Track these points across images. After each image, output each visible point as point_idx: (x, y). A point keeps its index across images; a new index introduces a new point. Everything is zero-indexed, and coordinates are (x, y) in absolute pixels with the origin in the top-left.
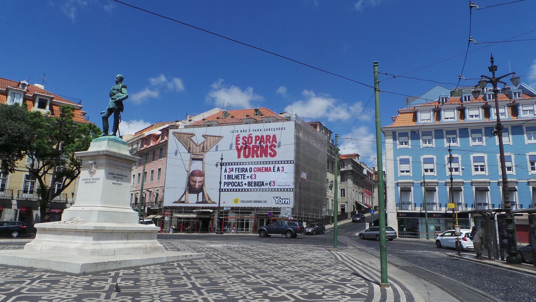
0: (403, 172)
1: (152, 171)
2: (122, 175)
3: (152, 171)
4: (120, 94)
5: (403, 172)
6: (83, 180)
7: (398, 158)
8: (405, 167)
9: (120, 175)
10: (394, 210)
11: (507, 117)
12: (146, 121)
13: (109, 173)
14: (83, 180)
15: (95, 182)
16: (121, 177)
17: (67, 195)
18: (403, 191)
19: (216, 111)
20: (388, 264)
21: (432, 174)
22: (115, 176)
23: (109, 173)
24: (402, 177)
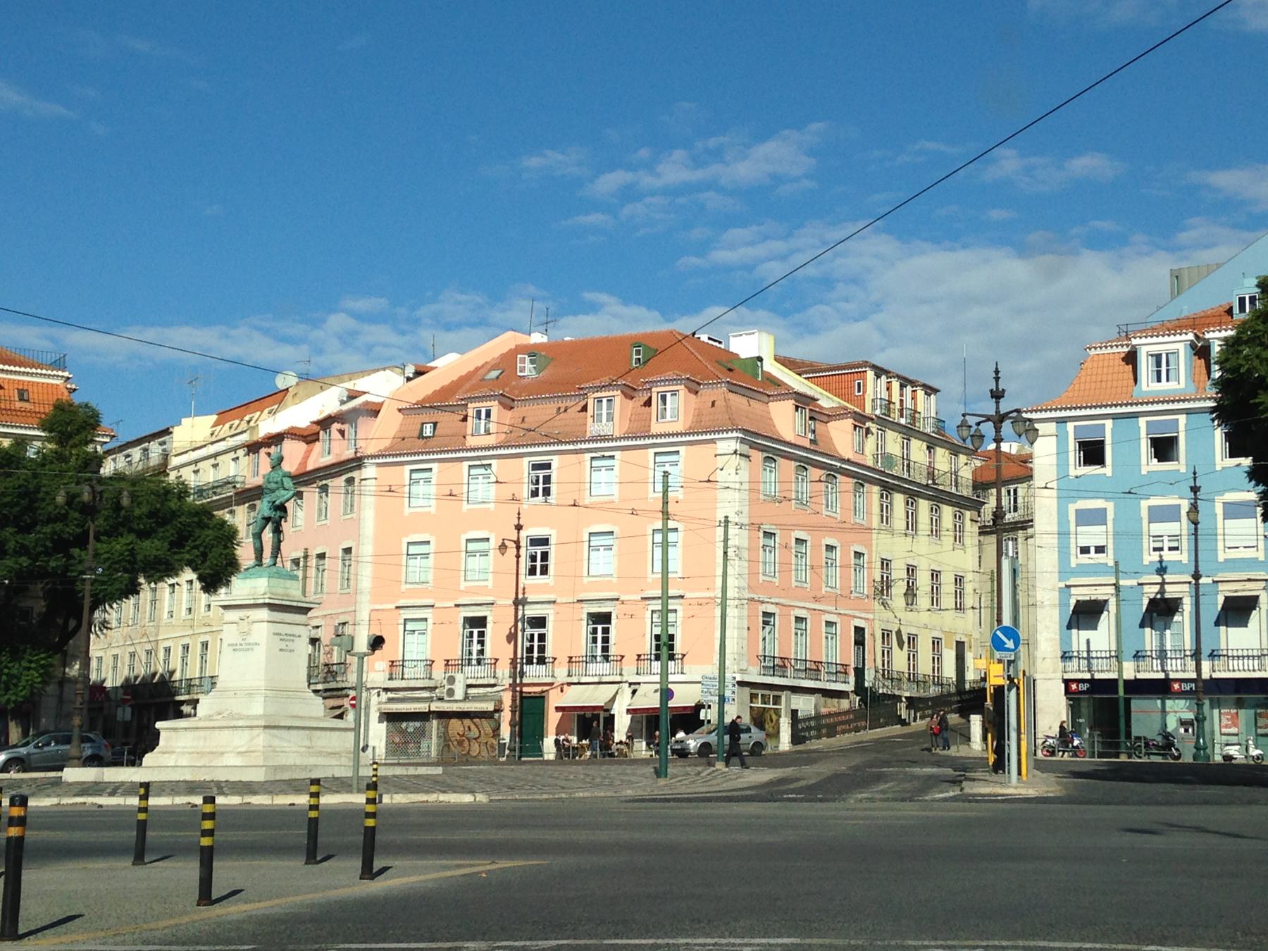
0: (1085, 550)
1: (186, 648)
2: (293, 635)
3: (186, 648)
4: (283, 492)
5: (1085, 550)
6: (229, 645)
7: (1072, 508)
8: (1092, 535)
9: (290, 635)
10: (1054, 672)
11: (1182, 385)
12: (726, 306)
13: (274, 634)
14: (229, 645)
15: (252, 649)
16: (292, 638)
17: (637, 674)
18: (1082, 613)
19: (302, 559)
20: (173, 679)
21: (1101, 557)
22: (282, 637)
23: (274, 634)
24: (1083, 570)
